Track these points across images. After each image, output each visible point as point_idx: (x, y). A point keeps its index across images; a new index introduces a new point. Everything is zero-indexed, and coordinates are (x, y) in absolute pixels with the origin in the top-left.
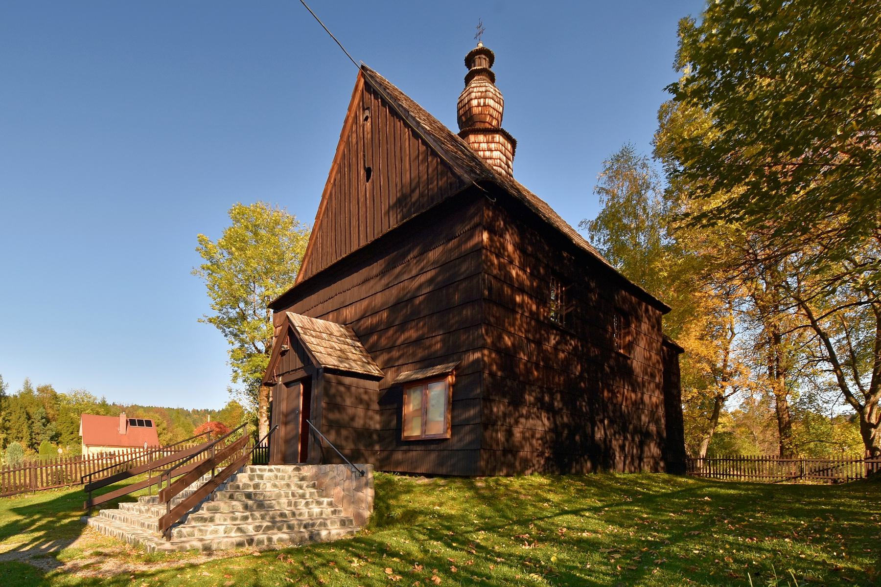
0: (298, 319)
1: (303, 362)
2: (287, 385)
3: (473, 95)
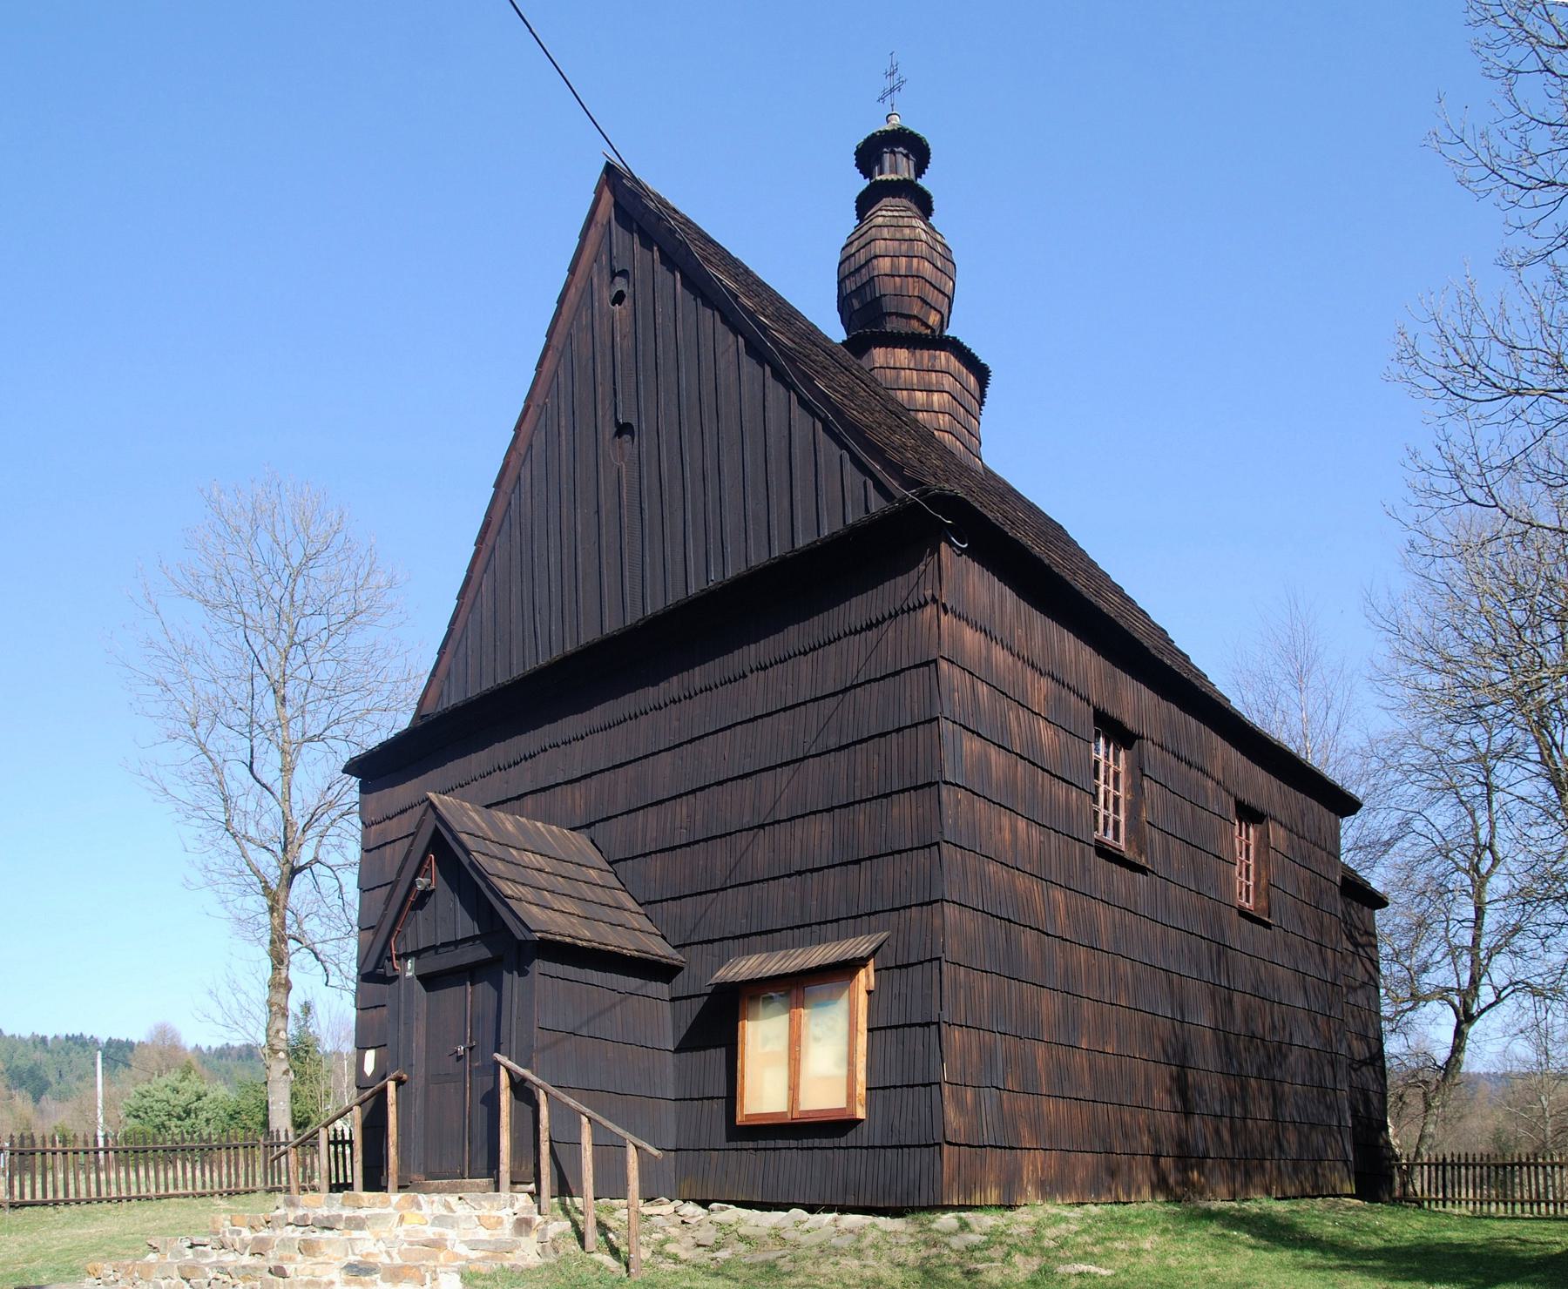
0: (466, 815)
1: (475, 916)
2: (430, 981)
3: (880, 247)
